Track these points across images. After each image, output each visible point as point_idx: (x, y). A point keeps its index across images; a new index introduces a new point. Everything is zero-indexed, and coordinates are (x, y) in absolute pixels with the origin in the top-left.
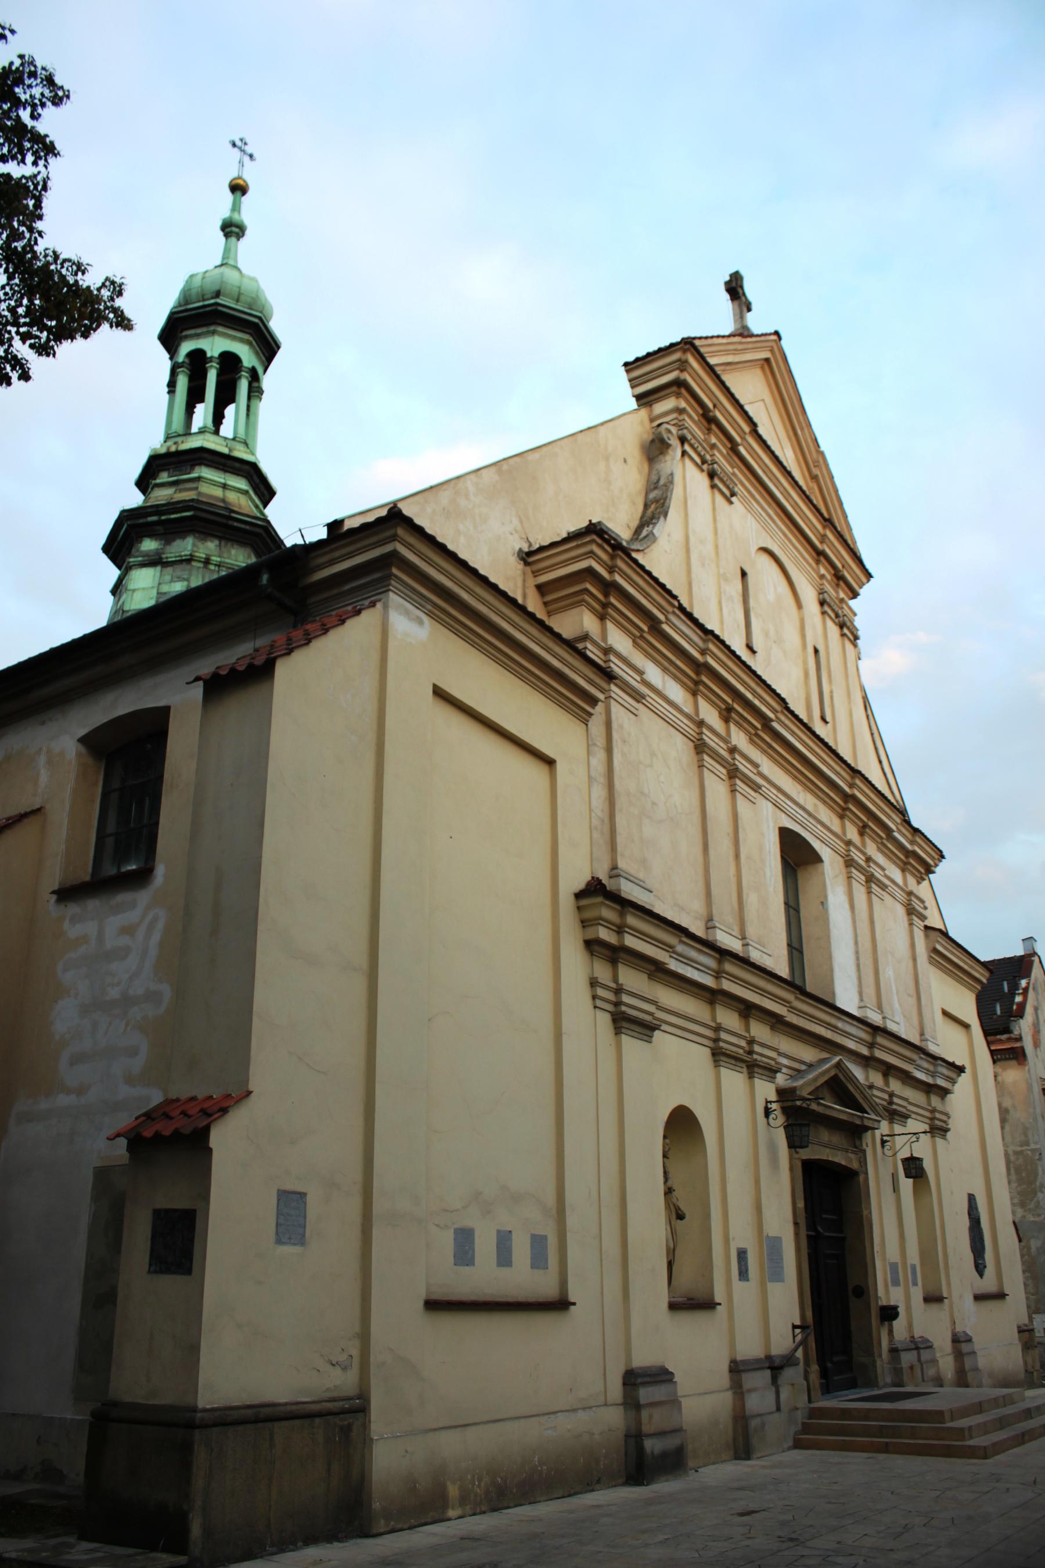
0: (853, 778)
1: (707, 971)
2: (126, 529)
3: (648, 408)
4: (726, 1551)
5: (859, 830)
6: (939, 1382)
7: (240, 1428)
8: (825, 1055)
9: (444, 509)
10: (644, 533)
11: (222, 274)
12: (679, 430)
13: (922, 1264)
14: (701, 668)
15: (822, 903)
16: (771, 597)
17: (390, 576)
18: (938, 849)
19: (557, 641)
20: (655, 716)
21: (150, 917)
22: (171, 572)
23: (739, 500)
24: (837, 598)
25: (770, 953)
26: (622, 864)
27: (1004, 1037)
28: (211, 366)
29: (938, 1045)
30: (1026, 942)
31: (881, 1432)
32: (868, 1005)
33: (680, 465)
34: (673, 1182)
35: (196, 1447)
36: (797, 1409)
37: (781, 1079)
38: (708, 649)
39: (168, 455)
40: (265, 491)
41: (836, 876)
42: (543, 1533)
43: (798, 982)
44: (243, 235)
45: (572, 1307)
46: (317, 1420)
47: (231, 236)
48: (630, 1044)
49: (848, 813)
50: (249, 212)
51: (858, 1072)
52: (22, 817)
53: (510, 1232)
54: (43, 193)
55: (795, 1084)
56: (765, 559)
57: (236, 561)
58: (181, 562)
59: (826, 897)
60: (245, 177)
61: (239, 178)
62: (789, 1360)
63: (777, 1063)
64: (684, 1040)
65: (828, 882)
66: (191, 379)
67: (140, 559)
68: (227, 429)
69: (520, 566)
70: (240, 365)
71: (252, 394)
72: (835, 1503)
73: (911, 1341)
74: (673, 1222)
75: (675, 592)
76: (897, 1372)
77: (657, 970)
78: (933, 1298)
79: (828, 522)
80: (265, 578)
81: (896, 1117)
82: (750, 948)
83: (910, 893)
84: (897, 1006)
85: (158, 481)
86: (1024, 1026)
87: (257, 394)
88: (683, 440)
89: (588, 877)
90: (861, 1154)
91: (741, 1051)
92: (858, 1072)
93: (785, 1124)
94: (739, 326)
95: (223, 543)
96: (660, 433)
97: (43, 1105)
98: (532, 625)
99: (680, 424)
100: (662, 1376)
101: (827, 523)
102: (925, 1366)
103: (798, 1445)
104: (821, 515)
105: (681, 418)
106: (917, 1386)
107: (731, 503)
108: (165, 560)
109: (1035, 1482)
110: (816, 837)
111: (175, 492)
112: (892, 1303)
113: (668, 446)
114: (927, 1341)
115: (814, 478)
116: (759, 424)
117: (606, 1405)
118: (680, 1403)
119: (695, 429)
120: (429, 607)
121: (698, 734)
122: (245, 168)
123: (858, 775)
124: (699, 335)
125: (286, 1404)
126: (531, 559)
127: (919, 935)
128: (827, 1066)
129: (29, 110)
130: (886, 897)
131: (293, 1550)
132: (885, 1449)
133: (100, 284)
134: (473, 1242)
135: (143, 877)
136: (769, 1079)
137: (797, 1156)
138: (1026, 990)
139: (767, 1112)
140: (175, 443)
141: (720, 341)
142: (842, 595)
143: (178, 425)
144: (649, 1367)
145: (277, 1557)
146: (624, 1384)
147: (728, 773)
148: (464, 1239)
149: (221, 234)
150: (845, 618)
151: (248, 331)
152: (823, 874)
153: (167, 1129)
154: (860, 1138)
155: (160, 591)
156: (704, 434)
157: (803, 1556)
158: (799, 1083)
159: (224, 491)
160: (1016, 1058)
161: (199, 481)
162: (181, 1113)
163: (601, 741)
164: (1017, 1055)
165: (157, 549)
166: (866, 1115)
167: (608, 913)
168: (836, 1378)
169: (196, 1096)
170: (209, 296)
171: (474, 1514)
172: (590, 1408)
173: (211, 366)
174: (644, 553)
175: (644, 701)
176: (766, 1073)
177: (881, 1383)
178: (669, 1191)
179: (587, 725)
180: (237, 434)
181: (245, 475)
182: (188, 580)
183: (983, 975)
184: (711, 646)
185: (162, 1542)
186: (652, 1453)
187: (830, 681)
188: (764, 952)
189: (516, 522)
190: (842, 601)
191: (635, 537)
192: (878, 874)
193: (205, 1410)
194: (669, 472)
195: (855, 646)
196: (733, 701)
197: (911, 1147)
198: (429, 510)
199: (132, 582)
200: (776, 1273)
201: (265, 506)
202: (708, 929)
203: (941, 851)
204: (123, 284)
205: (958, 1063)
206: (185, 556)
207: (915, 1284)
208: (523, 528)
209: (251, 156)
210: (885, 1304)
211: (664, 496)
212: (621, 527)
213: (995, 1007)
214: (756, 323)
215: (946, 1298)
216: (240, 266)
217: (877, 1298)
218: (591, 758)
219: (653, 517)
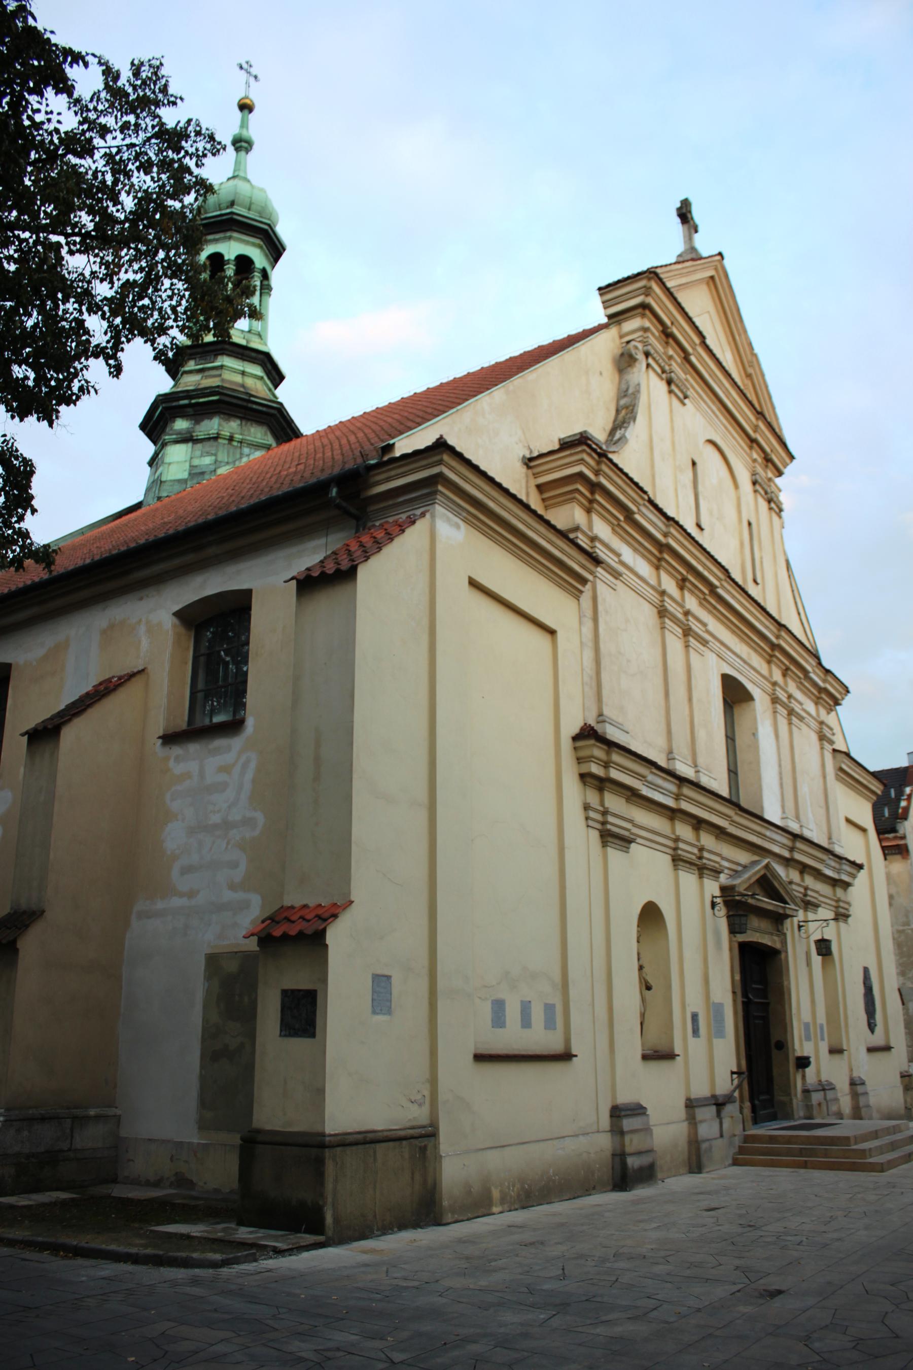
0: (779, 630)
2: (161, 411)
3: (618, 327)
6: (840, 1115)
7: (354, 1148)
8: (756, 858)
10: (618, 435)
11: (236, 185)
13: (828, 1023)
14: (663, 547)
15: (754, 734)
17: (436, 492)
20: (628, 589)
21: (243, 758)
22: (201, 448)
26: (606, 711)
27: (891, 836)
28: (229, 268)
31: (801, 1152)
34: (644, 962)
35: (327, 1161)
36: (735, 1135)
38: (670, 533)
40: (276, 376)
43: (734, 799)
45: (574, 1059)
46: (404, 1142)
47: (241, 150)
48: (613, 854)
49: (774, 659)
50: (256, 128)
51: (780, 870)
52: (131, 676)
56: (710, 449)
57: (255, 438)
58: (209, 439)
59: (756, 729)
60: (251, 96)
61: (246, 97)
63: (721, 866)
64: (652, 850)
67: (174, 437)
69: (524, 469)
70: (253, 267)
73: (819, 1084)
75: (646, 489)
76: (809, 1107)
77: (633, 795)
78: (835, 1051)
79: (760, 414)
80: (334, 492)
81: (810, 906)
82: (701, 774)
85: (186, 369)
87: (266, 291)
88: (647, 354)
89: (582, 724)
90: (782, 937)
91: (694, 857)
92: (780, 870)
94: (688, 247)
95: (244, 423)
96: (629, 349)
97: (160, 905)
98: (540, 524)
99: (645, 340)
100: (638, 1110)
101: (760, 416)
102: (829, 1103)
103: (736, 1163)
104: (755, 409)
105: (646, 335)
107: (684, 404)
108: (195, 438)
112: (806, 1054)
114: (831, 1084)
115: (749, 376)
117: (598, 1132)
119: (656, 344)
120: (465, 514)
123: (784, 629)
124: (660, 264)
125: (382, 1131)
126: (532, 464)
127: (828, 756)
128: (759, 867)
129: (194, 159)
130: (804, 727)
131: (391, 1234)
132: (805, 1165)
134: (504, 1010)
136: (714, 878)
137: (734, 939)
138: (909, 796)
139: (713, 905)
142: (770, 475)
144: (629, 1104)
145: (383, 1238)
146: (611, 1116)
147: (683, 632)
148: (499, 1007)
151: (258, 236)
152: (754, 710)
154: (782, 924)
156: (664, 348)
160: (900, 853)
163: (589, 613)
165: (188, 428)
166: (787, 906)
167: (598, 752)
168: (761, 1112)
172: (588, 1134)
175: (621, 578)
176: (713, 874)
177: (796, 1116)
178: (641, 968)
179: (578, 600)
182: (215, 455)
183: (877, 787)
184: (672, 530)
186: (633, 1167)
187: (760, 549)
190: (770, 480)
191: (610, 438)
192: (797, 708)
193: (331, 1135)
194: (636, 383)
195: (780, 517)
197: (822, 931)
200: (720, 1033)
201: (276, 387)
202: (669, 760)
203: (847, 688)
205: (858, 861)
206: (213, 434)
207: (823, 1039)
209: (256, 77)
212: (599, 434)
213: (883, 811)
214: (705, 245)
216: (249, 177)
217: (794, 1050)
219: (624, 422)
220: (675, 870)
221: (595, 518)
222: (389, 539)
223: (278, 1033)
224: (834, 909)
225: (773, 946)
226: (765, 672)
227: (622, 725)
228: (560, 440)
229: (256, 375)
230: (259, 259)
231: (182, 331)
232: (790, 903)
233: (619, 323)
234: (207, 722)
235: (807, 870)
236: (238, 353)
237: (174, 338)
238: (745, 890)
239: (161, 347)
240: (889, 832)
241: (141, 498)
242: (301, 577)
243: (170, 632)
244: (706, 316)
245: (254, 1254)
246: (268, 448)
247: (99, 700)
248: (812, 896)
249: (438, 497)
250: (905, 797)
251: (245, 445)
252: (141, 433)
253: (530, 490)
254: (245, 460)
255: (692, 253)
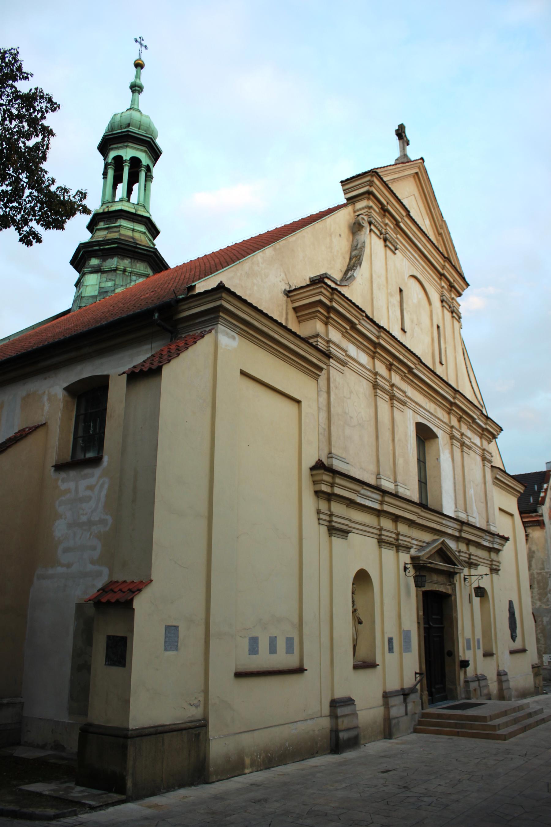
0: (455, 394)
1: (376, 501)
2: (82, 253)
3: (353, 205)
4: (373, 793)
5: (458, 419)
6: (489, 697)
8: (437, 537)
9: (246, 273)
10: (349, 275)
12: (368, 218)
15: (437, 459)
16: (415, 301)
17: (219, 317)
18: (499, 426)
19: (303, 342)
20: (353, 372)
22: (106, 277)
23: (400, 252)
24: (450, 298)
25: (409, 489)
26: (333, 451)
27: (534, 514)
28: (126, 165)
29: (496, 527)
30: (548, 464)
31: (456, 726)
32: (460, 510)
33: (369, 237)
35: (129, 747)
36: (416, 713)
37: (413, 552)
38: (381, 336)
39: (104, 213)
40: (154, 231)
41: (445, 445)
42: (289, 782)
43: (424, 502)
44: (142, 92)
45: (306, 672)
46: (184, 732)
47: (135, 92)
49: (452, 412)
52: (37, 428)
53: (276, 637)
54: (47, 150)
55: (420, 554)
56: (413, 280)
57: (140, 270)
58: (111, 271)
59: (439, 456)
60: (142, 59)
61: (140, 59)
62: (413, 690)
65: (441, 448)
66: (115, 171)
67: (90, 269)
68: (134, 198)
69: (285, 298)
70: (141, 164)
71: (147, 179)
72: (428, 766)
73: (476, 677)
74: (356, 626)
75: (363, 309)
77: (351, 503)
78: (488, 654)
79: (447, 259)
80: (156, 315)
81: (472, 566)
82: (399, 487)
83: (484, 450)
84: (475, 508)
85: (99, 227)
86: (544, 510)
87: (150, 179)
88: (370, 223)
89: (317, 459)
90: (453, 586)
91: (392, 540)
92: (452, 544)
93: (414, 575)
94: (402, 154)
95: (133, 261)
96: (359, 220)
97: (50, 571)
99: (369, 214)
100: (349, 702)
101: (446, 259)
102: (482, 688)
103: (415, 731)
105: (369, 211)
106: (477, 699)
107: (395, 254)
108: (103, 270)
109: (526, 754)
110: (435, 425)
111: (108, 233)
112: (467, 659)
113: (363, 227)
114: (484, 676)
115: (440, 234)
116: (411, 211)
117: (321, 717)
118: (357, 714)
119: (377, 217)
120: (238, 330)
121: (375, 379)
122: (142, 54)
125: (170, 725)
126: (290, 295)
127: (488, 471)
131: (173, 791)
132: (457, 734)
133: (75, 194)
134: (258, 644)
135: (96, 461)
136: (406, 552)
138: (546, 490)
139: (405, 569)
140: (107, 207)
141: (392, 167)
143: (108, 197)
145: (167, 795)
146: (331, 706)
148: (254, 642)
149: (130, 91)
150: (454, 308)
152: (438, 444)
153: (113, 598)
154: (453, 578)
155: (100, 287)
156: (382, 219)
157: (408, 797)
158: (420, 554)
159: (133, 233)
161: (120, 227)
162: (119, 590)
163: (324, 388)
164: (540, 524)
165: (99, 264)
166: (456, 567)
167: (327, 477)
168: (436, 696)
169: (126, 581)
170: (124, 126)
171: (257, 771)
172: (313, 718)
173: (126, 165)
174: (349, 286)
175: (347, 365)
176: (405, 549)
177: (459, 698)
178: (354, 611)
179: (317, 381)
180: (139, 201)
181: (144, 223)
182: (115, 281)
183: (521, 489)
184: (382, 334)
185: (114, 789)
187: (445, 343)
188: (405, 488)
189: (283, 275)
192: (467, 442)
193: (133, 730)
194: (363, 241)
195: (459, 322)
196: (393, 360)
197: (479, 582)
198: (239, 274)
199: (86, 281)
201: (154, 239)
202: (377, 479)
203: (501, 428)
204: (86, 193)
205: (506, 536)
206: (113, 268)
207: (479, 648)
208: (287, 278)
209: (146, 47)
210: (463, 659)
211: (360, 254)
213: (530, 499)
214: (413, 153)
215: (495, 654)
217: (459, 656)
218: (319, 398)
219: (354, 266)
220: (380, 548)
221: (330, 328)
222: (186, 348)
223: (104, 663)
224: (489, 566)
225: (447, 592)
226: (446, 420)
227: (345, 459)
228: (310, 278)
229: (141, 231)
230: (145, 159)
231: (38, 223)
232: (458, 565)
233: (354, 203)
234: (82, 457)
235: (471, 543)
236: (130, 218)
237: (32, 227)
238: (427, 559)
239: (25, 233)
240: (533, 512)
241: (70, 307)
242: (129, 373)
243: (61, 401)
244: (413, 197)
245: (75, 810)
246: (147, 276)
247: (16, 443)
248: (474, 559)
249: (220, 320)
250: (543, 490)
251: (133, 274)
252: (71, 267)
253: (288, 311)
254: (133, 283)
255: (404, 158)
